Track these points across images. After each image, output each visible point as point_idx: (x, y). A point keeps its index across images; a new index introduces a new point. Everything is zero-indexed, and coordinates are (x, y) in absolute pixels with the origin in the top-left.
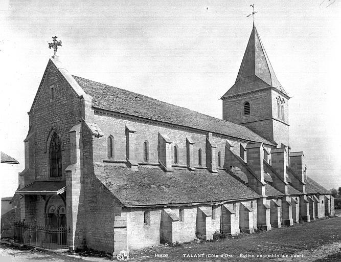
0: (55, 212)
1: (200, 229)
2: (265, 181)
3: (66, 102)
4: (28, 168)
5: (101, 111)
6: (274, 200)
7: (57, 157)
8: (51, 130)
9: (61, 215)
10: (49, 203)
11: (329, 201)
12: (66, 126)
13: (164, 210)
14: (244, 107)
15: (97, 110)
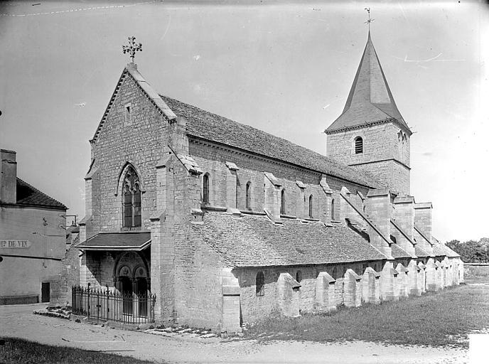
0: (130, 275)
3: (149, 127)
4: (91, 214)
10: (120, 262)
12: (148, 160)
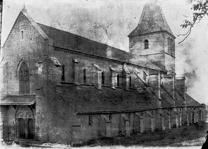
1: (200, 115)
2: (175, 97)
5: (71, 52)
6: (166, 111)
7: (25, 79)
8: (21, 60)
9: (28, 119)
11: (202, 112)
13: (100, 116)
14: (144, 44)
15: (56, 48)
